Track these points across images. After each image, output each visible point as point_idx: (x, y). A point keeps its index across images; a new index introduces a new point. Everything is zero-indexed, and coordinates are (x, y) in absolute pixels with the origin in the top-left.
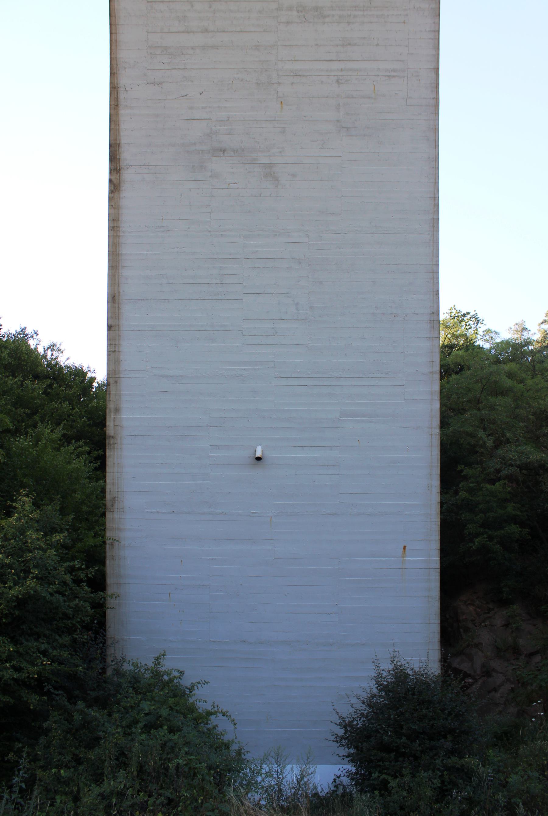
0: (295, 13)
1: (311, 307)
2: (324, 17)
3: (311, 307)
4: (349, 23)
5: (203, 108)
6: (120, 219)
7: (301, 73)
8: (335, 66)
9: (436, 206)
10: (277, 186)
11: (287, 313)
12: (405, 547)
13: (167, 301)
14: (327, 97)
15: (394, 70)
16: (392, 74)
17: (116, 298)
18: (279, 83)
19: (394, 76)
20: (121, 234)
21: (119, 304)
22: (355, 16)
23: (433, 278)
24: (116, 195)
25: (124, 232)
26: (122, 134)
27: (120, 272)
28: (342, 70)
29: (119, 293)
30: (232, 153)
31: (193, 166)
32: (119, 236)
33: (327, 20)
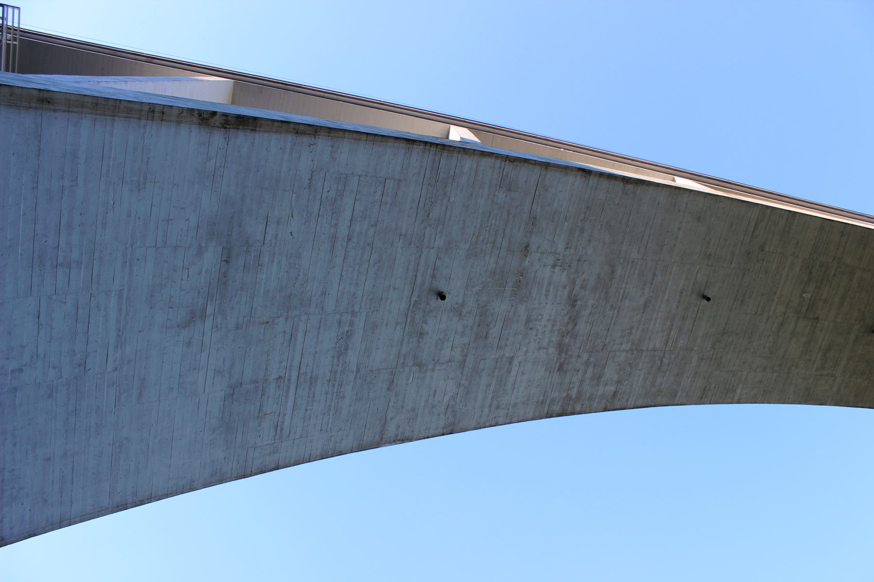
0: (347, 329)
1: (15, 389)
2: (338, 357)
3: (15, 389)
4: (329, 381)
5: (277, 235)
6: (164, 123)
7: (293, 340)
8: (294, 374)
9: (142, 503)
10: (178, 326)
11: (7, 358)
12: (708, 299)
13: (35, 185)
14: (266, 369)
15: (282, 429)
16: (279, 429)
17: (46, 106)
18: (287, 319)
19: (276, 431)
20: (143, 122)
21: (36, 108)
22: (334, 386)
23: (52, 525)
24: (195, 119)
25: (145, 127)
26: (266, 135)
27: (88, 115)
28: (289, 380)
29: (55, 111)
30: (222, 271)
31: (215, 224)
32: (140, 119)
33: (336, 359)
